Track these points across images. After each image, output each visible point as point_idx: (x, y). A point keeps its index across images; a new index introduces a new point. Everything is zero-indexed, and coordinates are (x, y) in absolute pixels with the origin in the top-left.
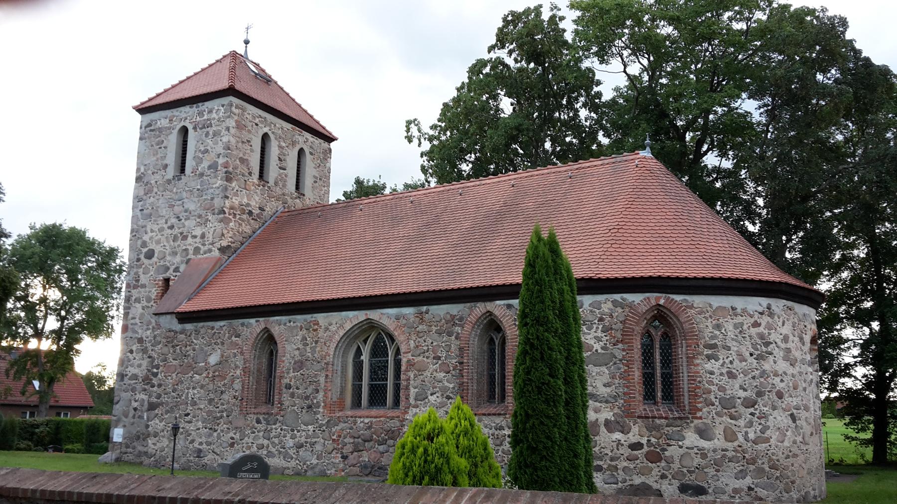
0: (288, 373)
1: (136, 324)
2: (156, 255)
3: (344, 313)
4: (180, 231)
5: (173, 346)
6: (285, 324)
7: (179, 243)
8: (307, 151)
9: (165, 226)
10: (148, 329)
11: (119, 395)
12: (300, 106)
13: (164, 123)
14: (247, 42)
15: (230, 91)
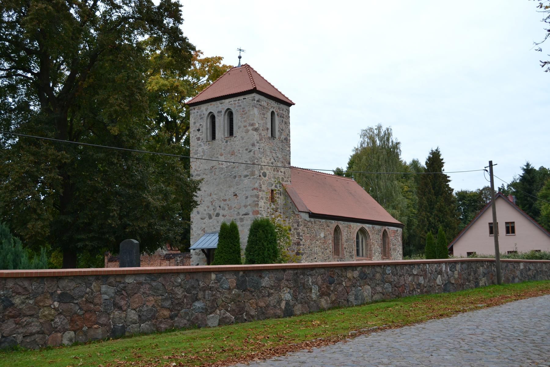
8: (276, 113)
12: (273, 87)
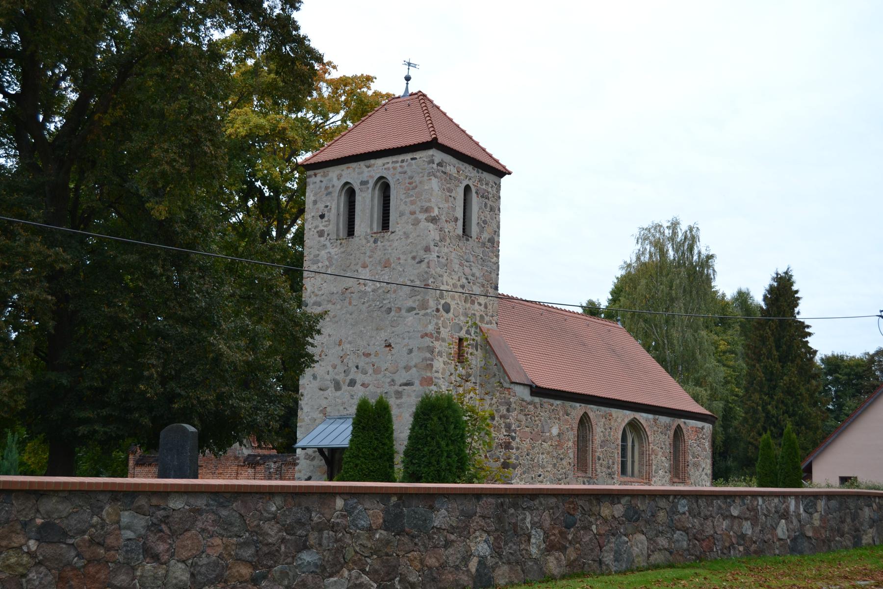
15: (433, 144)
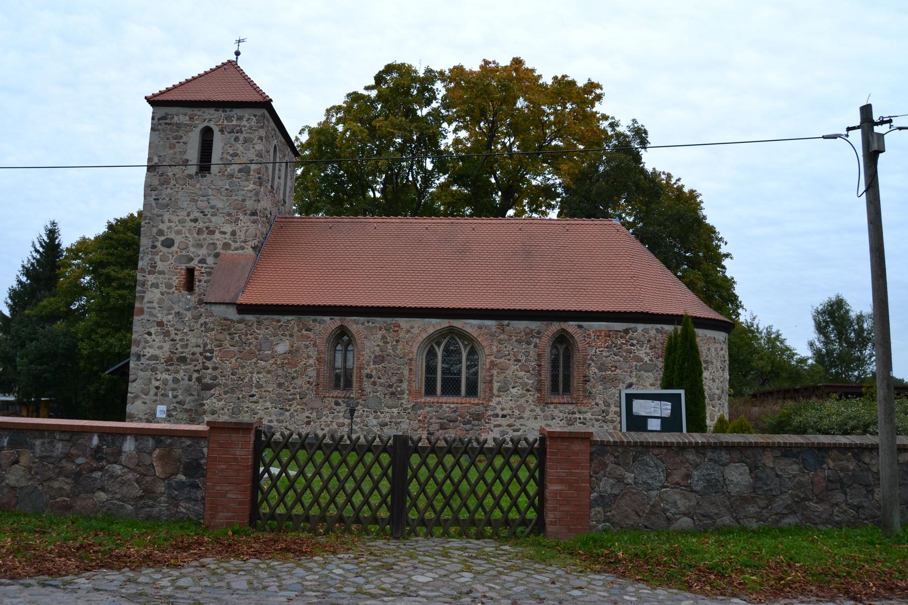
0: (368, 365)
1: (154, 308)
2: (176, 245)
3: (427, 320)
4: (207, 224)
5: (230, 334)
6: (363, 324)
7: (205, 236)
9: (188, 219)
10: (169, 314)
11: (135, 374)
13: (184, 119)
14: (237, 54)
